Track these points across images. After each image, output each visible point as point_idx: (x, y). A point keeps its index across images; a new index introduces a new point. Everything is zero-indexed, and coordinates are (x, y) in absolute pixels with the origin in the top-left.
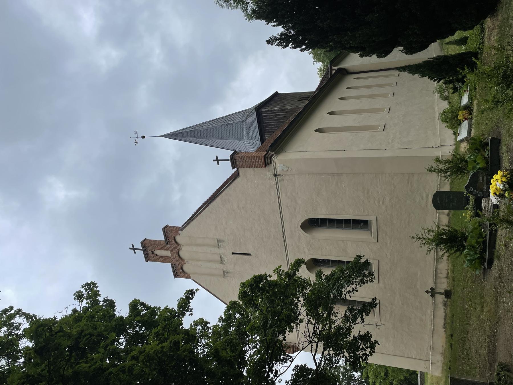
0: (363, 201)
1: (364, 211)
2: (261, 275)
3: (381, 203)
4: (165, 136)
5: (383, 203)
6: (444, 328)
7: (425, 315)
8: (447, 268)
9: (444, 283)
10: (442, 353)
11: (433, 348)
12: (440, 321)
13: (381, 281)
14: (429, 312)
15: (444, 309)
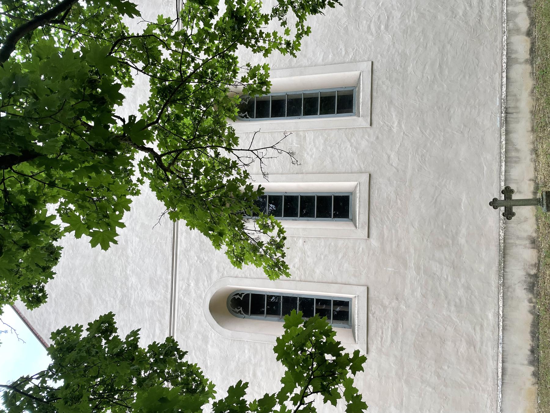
0: (346, 29)
1: (347, 52)
3: (383, 27)
5: (387, 27)
6: (531, 363)
8: (532, 175)
9: (526, 220)
12: (521, 342)
13: (374, 232)
14: (490, 316)
15: (530, 301)
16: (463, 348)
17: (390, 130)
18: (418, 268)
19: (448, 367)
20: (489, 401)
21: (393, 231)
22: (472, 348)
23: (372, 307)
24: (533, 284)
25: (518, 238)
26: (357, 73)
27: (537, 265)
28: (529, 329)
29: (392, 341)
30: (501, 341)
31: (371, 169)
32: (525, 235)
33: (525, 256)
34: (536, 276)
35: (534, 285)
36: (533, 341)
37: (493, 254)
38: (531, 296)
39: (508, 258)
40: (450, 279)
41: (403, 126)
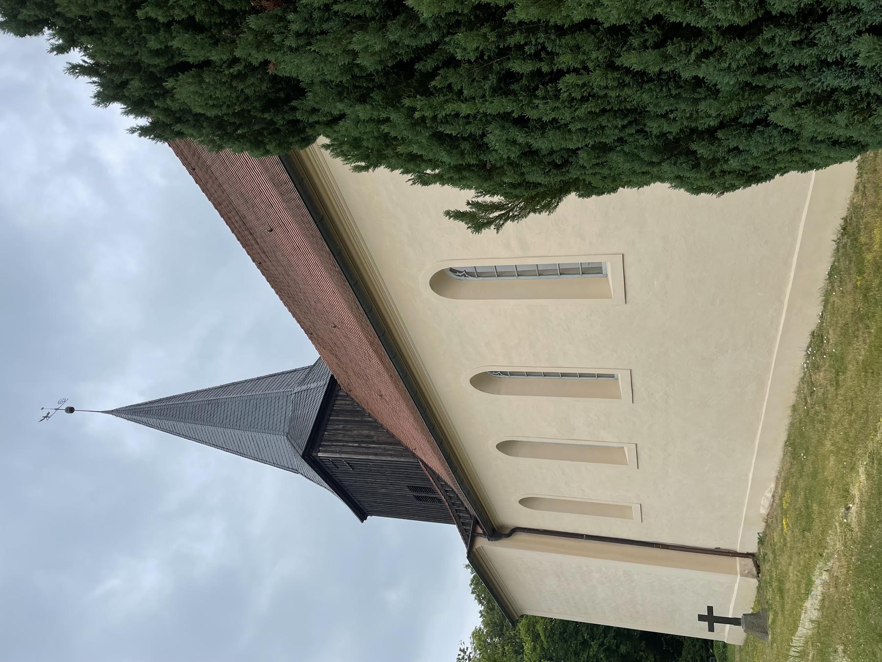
4: (117, 412)
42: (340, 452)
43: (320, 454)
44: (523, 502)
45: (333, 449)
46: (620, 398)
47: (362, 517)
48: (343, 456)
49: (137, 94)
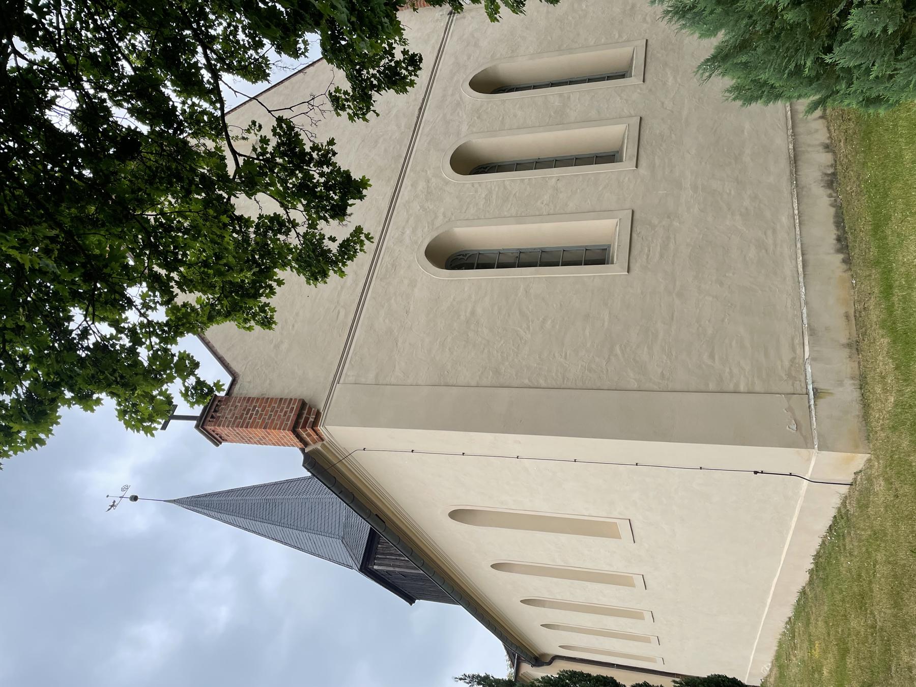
2: (347, 76)
4: (174, 501)
7: (774, 231)
9: (817, 131)
10: (849, 345)
11: (812, 332)
12: (823, 232)
13: (643, 162)
14: (784, 219)
15: (830, 196)
16: (752, 253)
17: (665, 84)
18: (695, 188)
19: (734, 274)
20: (789, 301)
21: (666, 161)
22: (764, 251)
23: (637, 228)
24: (831, 181)
25: (809, 145)
26: (630, 49)
27: (834, 166)
28: (832, 220)
29: (661, 256)
30: (798, 237)
31: (643, 114)
32: (817, 142)
33: (818, 161)
34: (834, 174)
35: (832, 182)
36: (838, 230)
37: (784, 165)
38: (829, 191)
39: (799, 163)
40: (733, 192)
41: (679, 80)
42: (394, 566)
43: (375, 567)
44: (455, 515)
45: (387, 562)
46: (643, 619)
47: (411, 600)
48: (397, 569)
49: (142, 306)
